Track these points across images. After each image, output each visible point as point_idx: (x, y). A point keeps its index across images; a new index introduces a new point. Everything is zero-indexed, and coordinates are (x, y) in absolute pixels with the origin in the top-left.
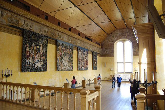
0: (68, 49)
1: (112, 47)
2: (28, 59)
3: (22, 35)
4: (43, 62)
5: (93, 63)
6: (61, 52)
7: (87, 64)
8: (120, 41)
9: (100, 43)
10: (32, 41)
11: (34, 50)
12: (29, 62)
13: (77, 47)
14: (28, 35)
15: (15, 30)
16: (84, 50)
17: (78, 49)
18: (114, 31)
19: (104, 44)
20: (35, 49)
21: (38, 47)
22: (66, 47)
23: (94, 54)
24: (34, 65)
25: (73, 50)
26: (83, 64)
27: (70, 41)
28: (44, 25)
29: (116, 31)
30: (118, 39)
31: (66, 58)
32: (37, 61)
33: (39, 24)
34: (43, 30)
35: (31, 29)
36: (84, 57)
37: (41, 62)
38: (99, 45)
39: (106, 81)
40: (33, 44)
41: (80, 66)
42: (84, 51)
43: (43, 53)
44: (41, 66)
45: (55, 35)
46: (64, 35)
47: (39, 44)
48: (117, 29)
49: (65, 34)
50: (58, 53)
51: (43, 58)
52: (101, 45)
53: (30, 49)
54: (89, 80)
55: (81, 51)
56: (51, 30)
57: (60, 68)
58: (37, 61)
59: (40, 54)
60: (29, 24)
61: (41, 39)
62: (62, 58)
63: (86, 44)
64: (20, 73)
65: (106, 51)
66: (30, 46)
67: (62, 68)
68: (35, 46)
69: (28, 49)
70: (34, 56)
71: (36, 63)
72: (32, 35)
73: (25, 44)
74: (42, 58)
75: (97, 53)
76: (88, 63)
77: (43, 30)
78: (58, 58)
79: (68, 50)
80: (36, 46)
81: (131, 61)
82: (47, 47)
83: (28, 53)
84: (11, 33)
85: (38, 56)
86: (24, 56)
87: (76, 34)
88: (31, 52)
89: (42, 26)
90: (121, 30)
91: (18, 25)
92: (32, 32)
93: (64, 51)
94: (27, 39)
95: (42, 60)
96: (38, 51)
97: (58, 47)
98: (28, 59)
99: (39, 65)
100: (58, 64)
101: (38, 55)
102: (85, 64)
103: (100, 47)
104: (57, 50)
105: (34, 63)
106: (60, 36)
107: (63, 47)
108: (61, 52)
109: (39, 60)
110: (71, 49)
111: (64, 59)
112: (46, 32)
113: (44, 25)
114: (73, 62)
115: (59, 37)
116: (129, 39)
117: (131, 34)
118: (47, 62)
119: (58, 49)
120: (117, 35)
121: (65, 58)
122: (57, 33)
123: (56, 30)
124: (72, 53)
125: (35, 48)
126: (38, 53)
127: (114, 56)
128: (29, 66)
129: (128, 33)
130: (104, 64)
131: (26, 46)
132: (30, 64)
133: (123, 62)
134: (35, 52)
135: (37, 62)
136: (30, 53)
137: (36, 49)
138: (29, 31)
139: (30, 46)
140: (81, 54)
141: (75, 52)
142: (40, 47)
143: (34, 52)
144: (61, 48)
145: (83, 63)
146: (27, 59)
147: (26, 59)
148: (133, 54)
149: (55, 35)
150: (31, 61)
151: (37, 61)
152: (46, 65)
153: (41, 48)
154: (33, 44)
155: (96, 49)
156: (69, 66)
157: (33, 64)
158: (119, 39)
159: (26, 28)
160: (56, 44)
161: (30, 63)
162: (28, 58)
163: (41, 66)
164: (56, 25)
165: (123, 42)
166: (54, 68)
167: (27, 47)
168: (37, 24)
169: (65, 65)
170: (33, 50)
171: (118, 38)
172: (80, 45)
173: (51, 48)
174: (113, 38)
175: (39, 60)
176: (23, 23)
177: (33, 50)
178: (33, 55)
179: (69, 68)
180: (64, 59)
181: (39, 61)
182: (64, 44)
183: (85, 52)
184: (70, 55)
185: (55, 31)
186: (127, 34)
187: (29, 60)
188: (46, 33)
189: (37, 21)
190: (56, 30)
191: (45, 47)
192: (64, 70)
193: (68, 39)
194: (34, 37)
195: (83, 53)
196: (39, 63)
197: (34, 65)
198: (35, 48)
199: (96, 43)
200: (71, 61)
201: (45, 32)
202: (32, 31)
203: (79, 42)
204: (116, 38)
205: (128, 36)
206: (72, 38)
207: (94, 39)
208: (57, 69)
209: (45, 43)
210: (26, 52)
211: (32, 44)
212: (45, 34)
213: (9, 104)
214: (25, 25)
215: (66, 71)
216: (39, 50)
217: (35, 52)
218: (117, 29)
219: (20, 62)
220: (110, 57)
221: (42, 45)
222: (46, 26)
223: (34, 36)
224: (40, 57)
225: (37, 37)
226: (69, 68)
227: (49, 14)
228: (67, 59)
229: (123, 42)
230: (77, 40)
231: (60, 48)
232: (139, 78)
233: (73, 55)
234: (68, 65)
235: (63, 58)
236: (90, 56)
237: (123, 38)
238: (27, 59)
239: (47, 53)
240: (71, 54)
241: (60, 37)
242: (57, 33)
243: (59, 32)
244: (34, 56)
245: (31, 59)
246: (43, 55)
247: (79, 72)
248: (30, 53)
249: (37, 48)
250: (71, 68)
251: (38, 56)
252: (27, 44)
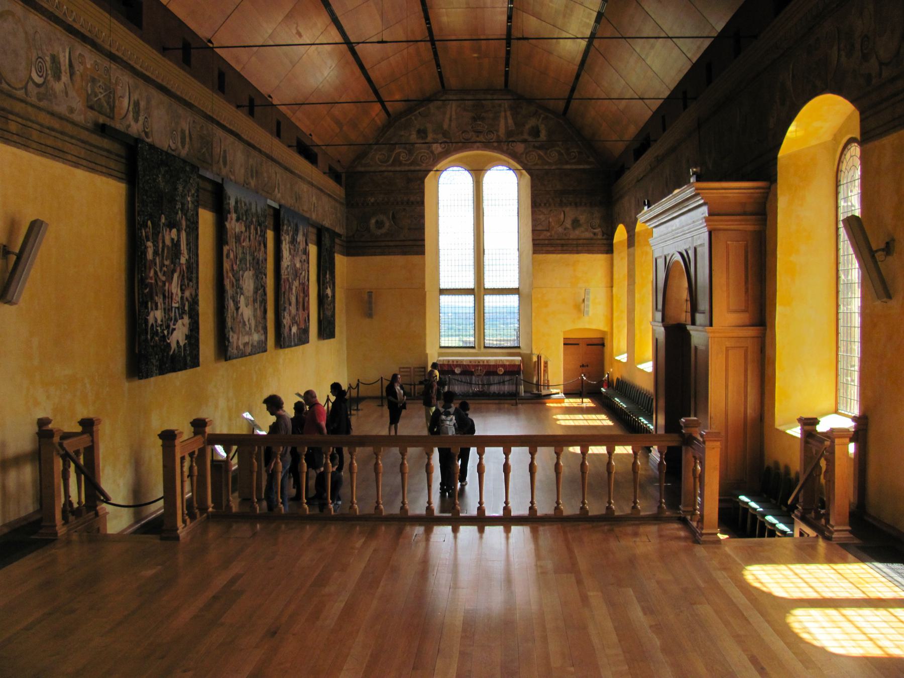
1: (412, 199)
3: (131, 177)
5: (322, 299)
18: (429, 100)
23: (326, 241)
25: (266, 228)
26: (293, 311)
30: (446, 154)
48: (444, 88)
52: (343, 176)
61: (180, 188)
64: (126, 385)
65: (377, 222)
75: (334, 235)
81: (515, 285)
91: (113, 118)
103: (339, 191)
116: (514, 156)
117: (528, 126)
120: (445, 126)
127: (422, 252)
129: (510, 121)
133: (488, 285)
136: (156, 272)
145: (293, 300)
148: (534, 245)
158: (457, 150)
160: (218, 203)
202: (149, 140)
205: (509, 134)
215: (250, 355)
220: (400, 260)
227: (217, 50)
232: (696, 359)
250: (263, 338)
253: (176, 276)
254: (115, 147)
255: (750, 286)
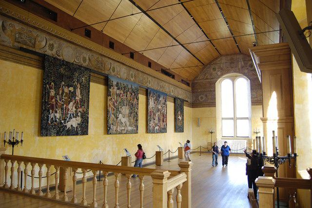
0: (128, 93)
1: (212, 90)
2: (53, 112)
3: (42, 66)
4: (82, 117)
5: (176, 119)
6: (116, 98)
7: (165, 120)
8: (227, 77)
9: (188, 82)
10: (61, 77)
11: (64, 94)
12: (55, 117)
13: (145, 90)
14: (54, 66)
15: (29, 58)
16: (159, 95)
17: (147, 93)
18: (216, 59)
19: (197, 83)
20: (66, 93)
21: (71, 89)
22: (124, 90)
23: (179, 102)
24: (65, 122)
25: (138, 94)
26: (156, 121)
27: (132, 78)
28: (83, 47)
29: (219, 59)
30: (222, 75)
31: (125, 110)
32: (69, 115)
33: (73, 46)
34: (82, 56)
35: (58, 55)
36: (160, 108)
37: (78, 118)
38: (188, 84)
39: (201, 153)
40: (63, 83)
41: (151, 124)
42: (159, 97)
43: (82, 100)
44: (78, 124)
45: (104, 65)
46: (122, 65)
47: (74, 84)
48: (221, 55)
49: (123, 64)
50: (110, 100)
51: (80, 110)
52: (190, 84)
53: (57, 94)
54: (169, 150)
55: (153, 96)
56: (96, 56)
57: (114, 128)
58: (70, 115)
59: (75, 102)
60: (55, 46)
61: (77, 75)
62: (117, 110)
63: (163, 83)
64: (38, 138)
65: (201, 97)
66: (57, 88)
67: (118, 129)
68: (66, 87)
69: (53, 93)
70: (65, 106)
71: (68, 119)
72: (61, 66)
73: (48, 83)
74: (78, 110)
75: (183, 101)
76: (166, 120)
77: (82, 56)
78: (110, 109)
79: (128, 95)
80: (69, 86)
81: (247, 116)
82: (89, 89)
83: (53, 100)
84: (20, 62)
85: (71, 107)
86: (45, 105)
87: (144, 64)
88: (58, 99)
89: (79, 49)
90: (229, 58)
91: (34, 47)
92: (60, 60)
93: (121, 96)
94: (51, 73)
95: (79, 114)
96: (72, 97)
97: (110, 88)
98: (53, 112)
99: (74, 123)
100: (110, 122)
101: (71, 103)
102: (161, 122)
103: (190, 89)
104: (108, 94)
105: (65, 120)
106: (114, 69)
107: (118, 89)
108: (116, 98)
109: (73, 114)
110: (135, 93)
111: (120, 112)
112: (88, 61)
113: (83, 47)
114: (137, 117)
115: (111, 70)
116: (244, 74)
117: (248, 64)
118: (88, 118)
119: (110, 93)
120: (222, 67)
121: (124, 110)
122: (108, 62)
123: (105, 56)
124: (136, 100)
125: (66, 90)
126: (71, 101)
127: (215, 106)
128: (55, 124)
129: (243, 63)
130: (197, 122)
131: (49, 88)
132: (56, 121)
134: (66, 98)
135: (70, 118)
136: (56, 100)
137: (68, 92)
138: (54, 58)
139: (57, 88)
140: (153, 101)
141: (142, 98)
142: (75, 89)
143: (64, 98)
144: (115, 90)
145: (157, 118)
146: (51, 111)
147: (48, 111)
148: (252, 103)
149: (104, 65)
150: (58, 115)
151: (69, 115)
152: (88, 123)
153: (78, 92)
154: (63, 83)
155: (182, 92)
156: (130, 125)
157: (63, 122)
158: (225, 74)
159: (49, 52)
161: (58, 120)
162: (53, 109)
163: (78, 124)
164: (106, 46)
165: (233, 79)
166: (101, 129)
167: (51, 88)
168: (71, 45)
169: (124, 123)
170: (62, 94)
171: (224, 72)
172: (152, 84)
173: (97, 91)
174: (214, 72)
175: (73, 114)
176: (44, 43)
177: (62, 94)
178: (63, 105)
179: (130, 128)
180: (120, 112)
181: (75, 115)
182: (121, 84)
183: (161, 99)
184: (132, 104)
185: (104, 59)
186: (241, 64)
187: (56, 114)
188: (87, 63)
189: (69, 40)
190: (105, 56)
191: (86, 90)
192: (120, 133)
193: (128, 75)
194: (65, 69)
195: (157, 100)
196: (74, 119)
197: (65, 122)
198: (66, 90)
199: (182, 80)
200: (134, 115)
201: (84, 60)
202: (61, 58)
203: (150, 78)
204: (218, 71)
205: (242, 67)
206: (137, 72)
207: (178, 73)
208: (108, 130)
209: (86, 81)
210: (48, 98)
211: (61, 82)
212: (85, 65)
213: (17, 197)
214: (47, 48)
215: (125, 133)
216: (73, 94)
217: (66, 98)
218: (221, 55)
219: (37, 117)
220: (208, 109)
221: (79, 86)
222: (86, 49)
223: (64, 67)
224: (76, 108)
225: (70, 69)
226: (130, 128)
227: (93, 26)
228: (127, 111)
229: (233, 79)
230: (145, 76)
231: (114, 90)
233: (138, 104)
234: (128, 124)
235: (120, 109)
236: (170, 106)
237: (232, 71)
238: (51, 111)
239: (88, 101)
240: (134, 103)
241: (114, 71)
242: (108, 63)
243: (111, 61)
244: (65, 106)
245: (58, 111)
246: (82, 104)
247: (150, 135)
248: (56, 100)
249: (70, 91)
250: (135, 129)
251: (71, 107)
252: (51, 84)
253: (273, 166)
254: (103, 77)
255: (284, 93)
